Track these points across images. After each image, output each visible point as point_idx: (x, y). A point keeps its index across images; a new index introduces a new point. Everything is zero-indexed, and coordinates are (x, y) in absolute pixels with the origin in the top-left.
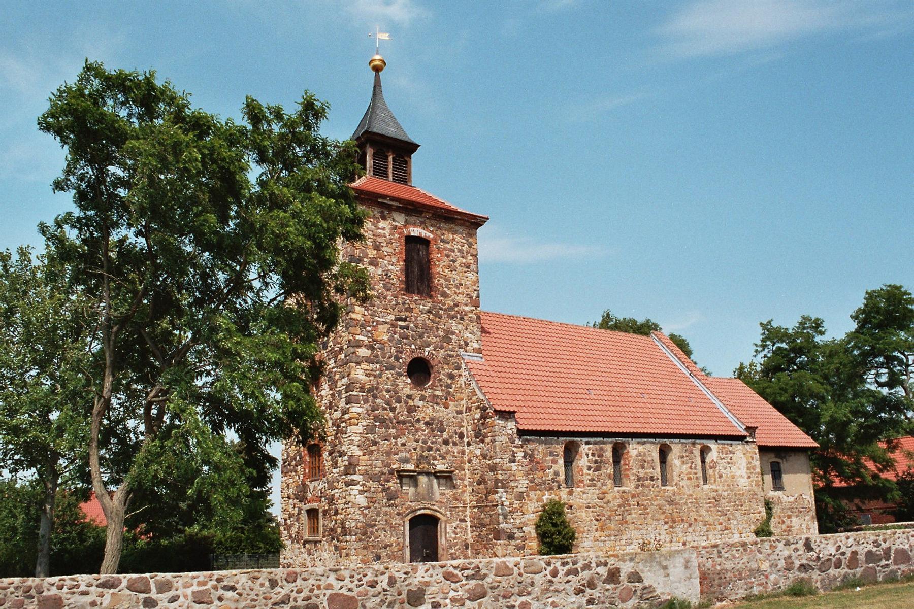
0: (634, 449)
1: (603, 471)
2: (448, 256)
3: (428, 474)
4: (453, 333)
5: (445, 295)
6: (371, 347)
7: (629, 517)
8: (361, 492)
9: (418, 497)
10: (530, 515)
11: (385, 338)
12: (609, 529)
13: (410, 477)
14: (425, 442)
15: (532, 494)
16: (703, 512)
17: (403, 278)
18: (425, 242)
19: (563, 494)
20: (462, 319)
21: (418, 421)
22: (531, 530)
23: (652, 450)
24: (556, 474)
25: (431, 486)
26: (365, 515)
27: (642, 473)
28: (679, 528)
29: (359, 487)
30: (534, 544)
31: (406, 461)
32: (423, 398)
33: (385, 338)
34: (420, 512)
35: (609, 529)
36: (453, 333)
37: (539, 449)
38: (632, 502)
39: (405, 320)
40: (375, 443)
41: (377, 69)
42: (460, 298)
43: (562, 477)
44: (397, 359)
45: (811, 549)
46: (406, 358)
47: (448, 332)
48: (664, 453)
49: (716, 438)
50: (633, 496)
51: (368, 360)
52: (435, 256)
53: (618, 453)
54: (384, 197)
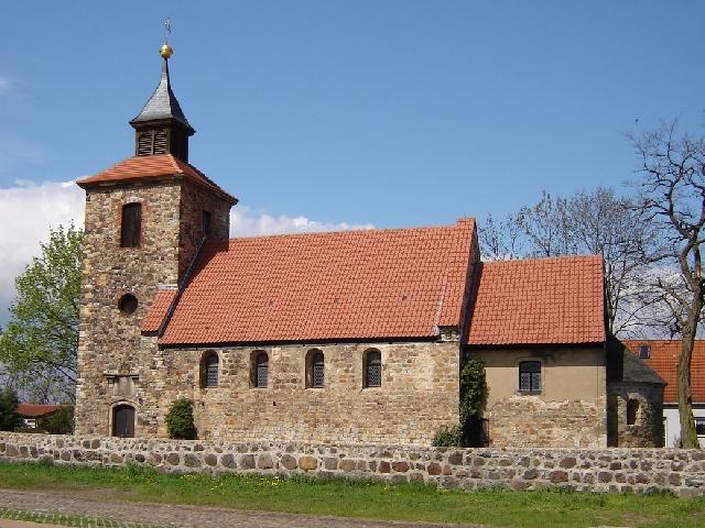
0: (275, 353)
1: (240, 374)
2: (154, 212)
3: (127, 376)
4: (155, 271)
5: (150, 243)
6: (94, 292)
7: (261, 414)
8: (83, 389)
9: (119, 392)
10: (165, 406)
11: (104, 283)
12: (239, 423)
13: (116, 379)
14: (128, 355)
15: (167, 392)
16: (356, 414)
17: (119, 237)
18: (137, 205)
19: (196, 393)
20: (163, 259)
21: (124, 339)
22: (161, 418)
23: (298, 355)
24: (191, 377)
25: (128, 385)
26: (84, 404)
27: (281, 376)
28: (322, 428)
29: (82, 386)
30: (163, 429)
31: (113, 368)
32: (128, 323)
33: (104, 283)
34: (120, 403)
35: (239, 423)
36: (155, 271)
37: (178, 355)
38: (267, 401)
39: (118, 268)
40: (93, 356)
41: (166, 57)
42: (162, 244)
43: (197, 378)
44: (111, 297)
45: (191, 433)
46: (117, 296)
47: (152, 270)
48: (315, 360)
49: (390, 340)
50: (270, 396)
51: (91, 301)
52: (145, 213)
53: (260, 359)
54: (102, 182)
